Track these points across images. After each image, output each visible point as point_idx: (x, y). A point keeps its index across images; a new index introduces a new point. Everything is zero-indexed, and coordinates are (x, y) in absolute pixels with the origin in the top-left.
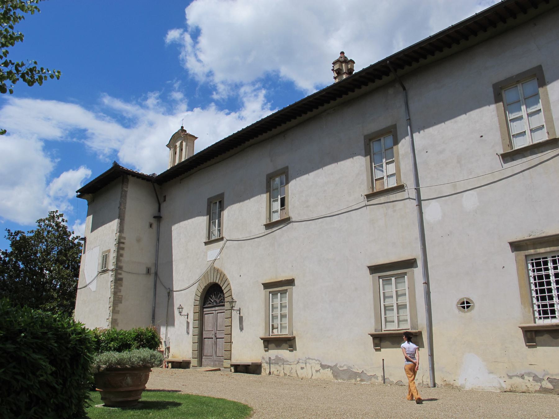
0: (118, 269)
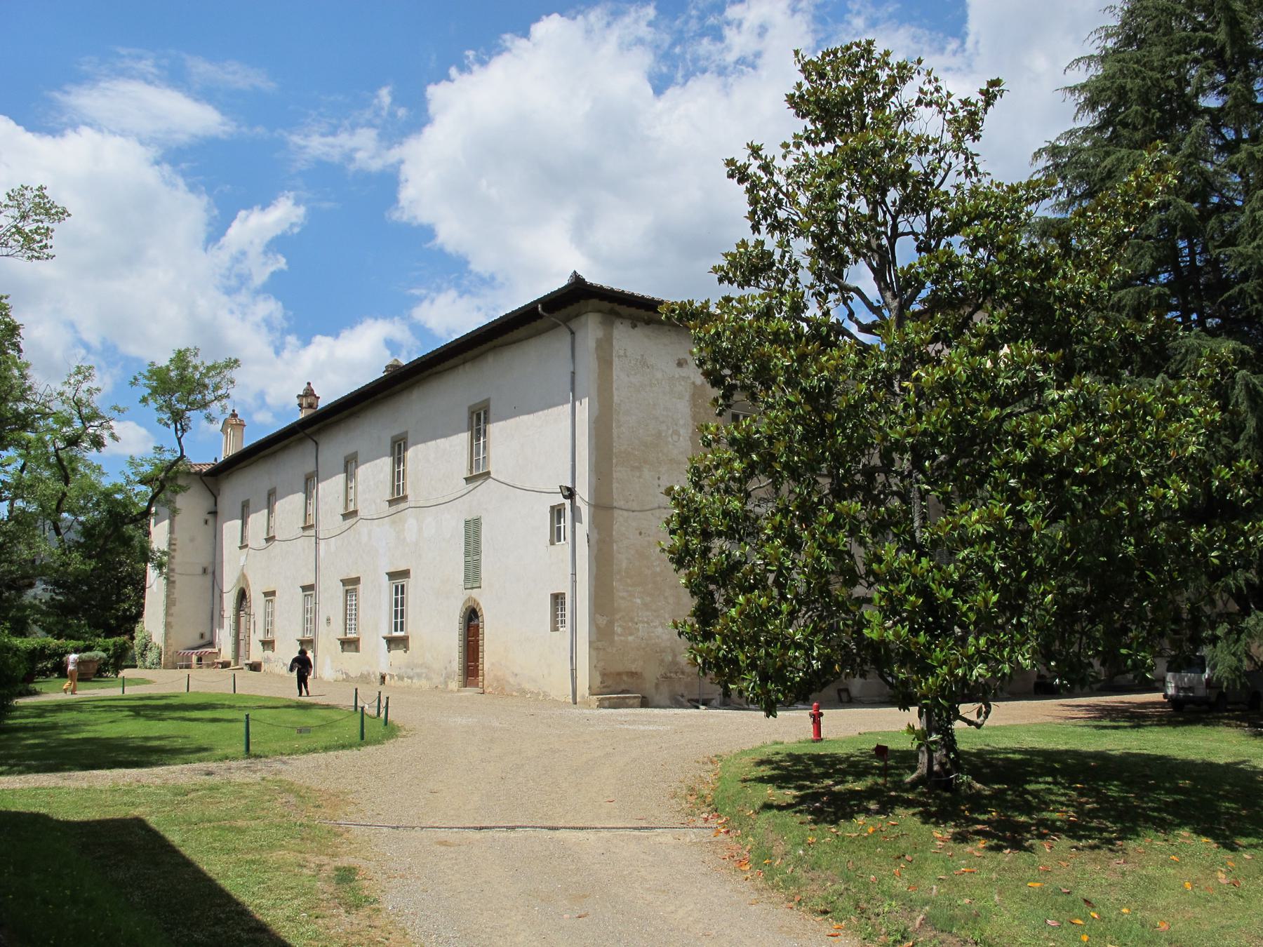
0: (602, 507)
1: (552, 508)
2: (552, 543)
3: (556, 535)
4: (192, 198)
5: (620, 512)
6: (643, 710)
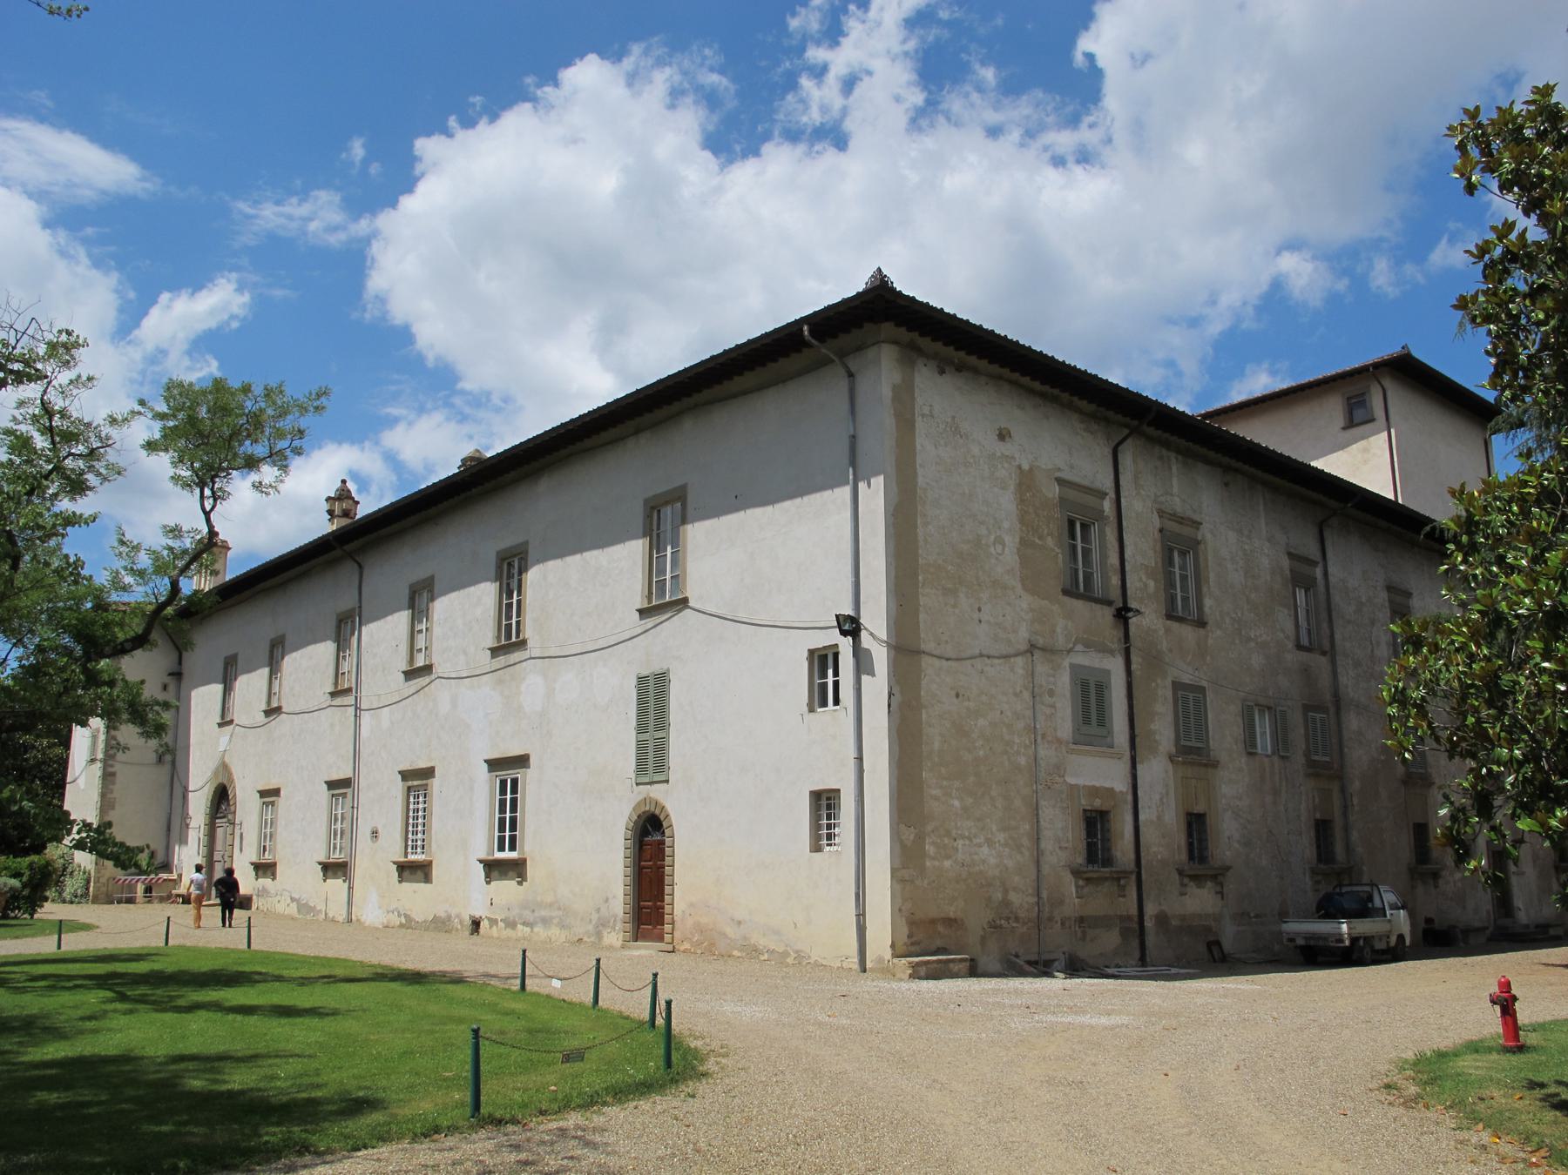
1: (811, 652)
2: (811, 710)
3: (820, 696)
4: (95, 274)
5: (930, 660)
6: (931, 984)
